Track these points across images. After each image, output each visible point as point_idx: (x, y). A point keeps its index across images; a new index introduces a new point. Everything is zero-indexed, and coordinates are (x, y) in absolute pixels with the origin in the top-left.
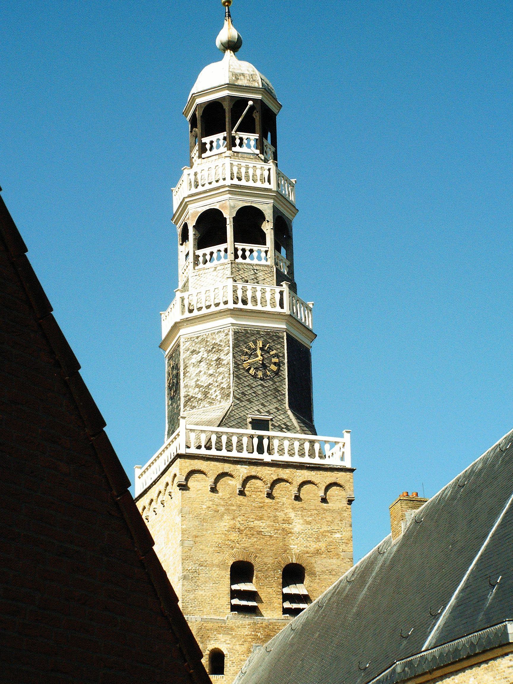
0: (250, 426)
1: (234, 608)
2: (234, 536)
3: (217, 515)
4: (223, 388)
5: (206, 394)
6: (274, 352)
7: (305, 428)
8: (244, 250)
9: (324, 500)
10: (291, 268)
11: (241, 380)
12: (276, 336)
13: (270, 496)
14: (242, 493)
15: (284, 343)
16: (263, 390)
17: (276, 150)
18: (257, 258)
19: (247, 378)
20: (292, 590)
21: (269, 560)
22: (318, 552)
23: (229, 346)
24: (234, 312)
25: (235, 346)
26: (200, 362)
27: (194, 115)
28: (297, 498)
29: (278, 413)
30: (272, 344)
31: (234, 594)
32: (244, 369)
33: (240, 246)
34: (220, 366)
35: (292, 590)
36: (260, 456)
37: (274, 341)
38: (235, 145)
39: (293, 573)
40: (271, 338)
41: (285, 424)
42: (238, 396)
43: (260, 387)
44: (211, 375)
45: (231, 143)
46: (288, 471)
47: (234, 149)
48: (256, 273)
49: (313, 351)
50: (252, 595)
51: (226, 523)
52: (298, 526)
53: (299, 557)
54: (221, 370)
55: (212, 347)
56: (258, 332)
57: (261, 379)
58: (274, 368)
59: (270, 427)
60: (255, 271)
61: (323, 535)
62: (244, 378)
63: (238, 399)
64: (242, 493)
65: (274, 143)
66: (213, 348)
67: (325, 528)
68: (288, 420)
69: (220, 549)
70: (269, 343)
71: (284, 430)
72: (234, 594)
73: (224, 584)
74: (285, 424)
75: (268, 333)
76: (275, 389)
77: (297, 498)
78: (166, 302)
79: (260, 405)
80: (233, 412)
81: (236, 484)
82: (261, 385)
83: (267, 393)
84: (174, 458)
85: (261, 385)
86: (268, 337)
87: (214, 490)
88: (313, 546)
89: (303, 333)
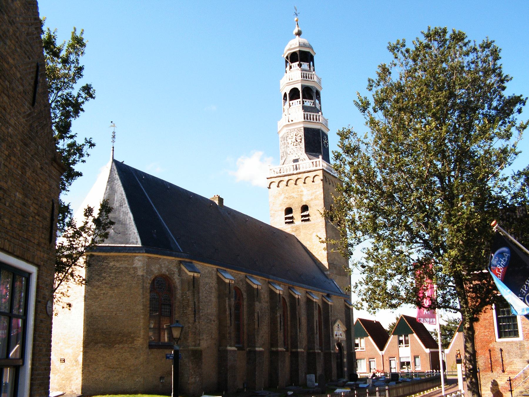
1: (286, 223)
2: (286, 200)
3: (280, 194)
9: (313, 182)
13: (296, 184)
14: (287, 185)
20: (305, 213)
21: (297, 205)
22: (312, 200)
24: (287, 126)
28: (304, 183)
31: (302, 216)
33: (304, 100)
35: (305, 213)
39: (305, 208)
45: (300, 65)
46: (301, 175)
50: (292, 218)
51: (283, 196)
52: (305, 192)
53: (306, 202)
61: (313, 193)
64: (287, 185)
67: (314, 191)
69: (281, 205)
72: (302, 216)
73: (283, 216)
77: (304, 183)
78: (64, 170)
81: (284, 183)
87: (278, 186)
88: (310, 198)
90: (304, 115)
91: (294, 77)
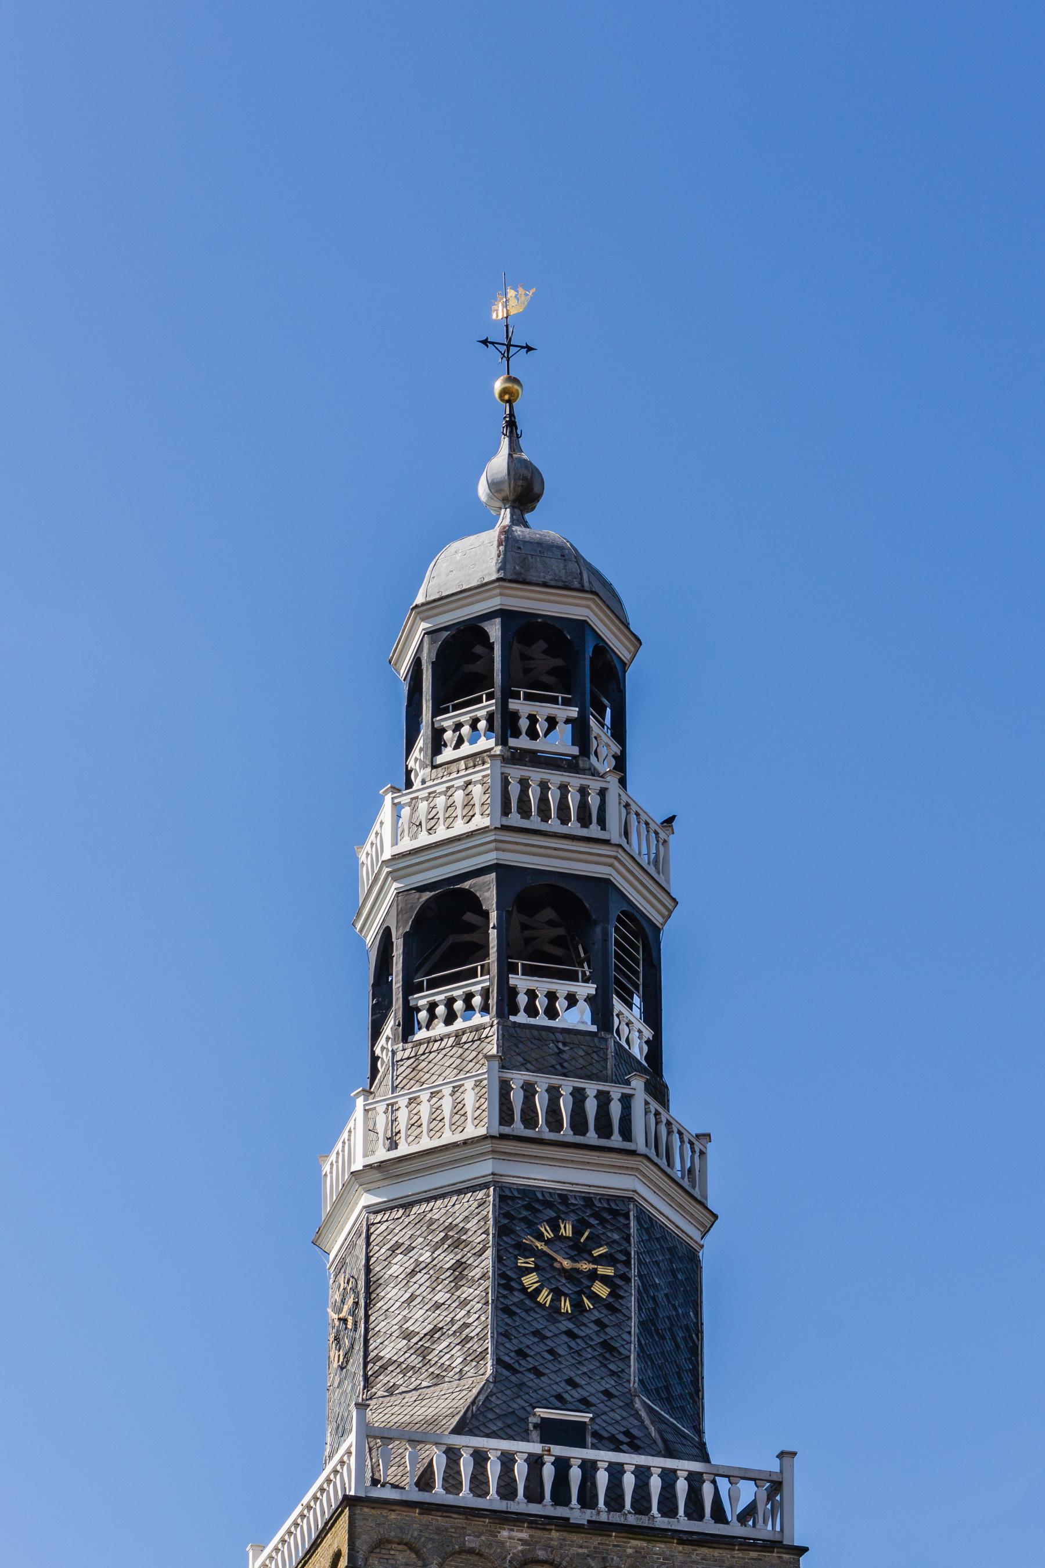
0: (535, 1435)
4: (468, 1339)
5: (423, 1353)
6: (603, 1250)
7: (619, 667)
8: (552, 996)
10: (655, 1047)
11: (517, 1318)
12: (611, 1211)
15: (629, 1228)
16: (572, 1344)
17: (623, 752)
18: (525, 1011)
19: (532, 1313)
23: (486, 1232)
25: (502, 1231)
26: (413, 1273)
27: (417, 662)
29: (609, 1403)
30: (600, 1230)
32: (524, 1290)
34: (464, 1281)
36: (561, 1512)
37: (603, 1221)
38: (517, 734)
40: (596, 1215)
41: (627, 1433)
42: (506, 1359)
43: (565, 1338)
44: (437, 1306)
47: (513, 742)
48: (561, 1051)
49: (706, 1257)
54: (466, 1292)
55: (442, 1234)
56: (564, 1198)
57: (570, 1317)
58: (601, 1290)
59: (589, 1440)
60: (560, 1045)
62: (523, 1315)
63: (508, 1367)
65: (619, 733)
66: (446, 1237)
68: (636, 1422)
70: (591, 1226)
71: (625, 1447)
74: (627, 1433)
75: (588, 1200)
76: (605, 1345)
79: (563, 1384)
80: (493, 1399)
82: (570, 1333)
83: (583, 1353)
84: (324, 1528)
85: (570, 1333)
86: (589, 1212)
89: (680, 1205)
90: (505, 1088)
91: (441, 806)
